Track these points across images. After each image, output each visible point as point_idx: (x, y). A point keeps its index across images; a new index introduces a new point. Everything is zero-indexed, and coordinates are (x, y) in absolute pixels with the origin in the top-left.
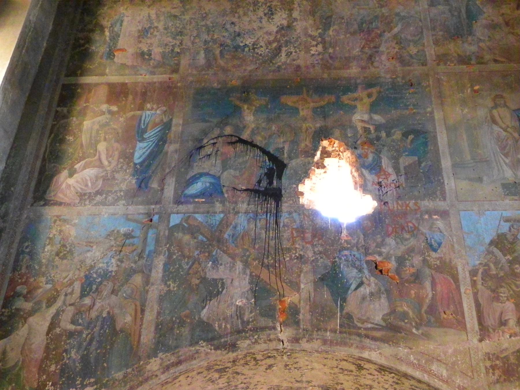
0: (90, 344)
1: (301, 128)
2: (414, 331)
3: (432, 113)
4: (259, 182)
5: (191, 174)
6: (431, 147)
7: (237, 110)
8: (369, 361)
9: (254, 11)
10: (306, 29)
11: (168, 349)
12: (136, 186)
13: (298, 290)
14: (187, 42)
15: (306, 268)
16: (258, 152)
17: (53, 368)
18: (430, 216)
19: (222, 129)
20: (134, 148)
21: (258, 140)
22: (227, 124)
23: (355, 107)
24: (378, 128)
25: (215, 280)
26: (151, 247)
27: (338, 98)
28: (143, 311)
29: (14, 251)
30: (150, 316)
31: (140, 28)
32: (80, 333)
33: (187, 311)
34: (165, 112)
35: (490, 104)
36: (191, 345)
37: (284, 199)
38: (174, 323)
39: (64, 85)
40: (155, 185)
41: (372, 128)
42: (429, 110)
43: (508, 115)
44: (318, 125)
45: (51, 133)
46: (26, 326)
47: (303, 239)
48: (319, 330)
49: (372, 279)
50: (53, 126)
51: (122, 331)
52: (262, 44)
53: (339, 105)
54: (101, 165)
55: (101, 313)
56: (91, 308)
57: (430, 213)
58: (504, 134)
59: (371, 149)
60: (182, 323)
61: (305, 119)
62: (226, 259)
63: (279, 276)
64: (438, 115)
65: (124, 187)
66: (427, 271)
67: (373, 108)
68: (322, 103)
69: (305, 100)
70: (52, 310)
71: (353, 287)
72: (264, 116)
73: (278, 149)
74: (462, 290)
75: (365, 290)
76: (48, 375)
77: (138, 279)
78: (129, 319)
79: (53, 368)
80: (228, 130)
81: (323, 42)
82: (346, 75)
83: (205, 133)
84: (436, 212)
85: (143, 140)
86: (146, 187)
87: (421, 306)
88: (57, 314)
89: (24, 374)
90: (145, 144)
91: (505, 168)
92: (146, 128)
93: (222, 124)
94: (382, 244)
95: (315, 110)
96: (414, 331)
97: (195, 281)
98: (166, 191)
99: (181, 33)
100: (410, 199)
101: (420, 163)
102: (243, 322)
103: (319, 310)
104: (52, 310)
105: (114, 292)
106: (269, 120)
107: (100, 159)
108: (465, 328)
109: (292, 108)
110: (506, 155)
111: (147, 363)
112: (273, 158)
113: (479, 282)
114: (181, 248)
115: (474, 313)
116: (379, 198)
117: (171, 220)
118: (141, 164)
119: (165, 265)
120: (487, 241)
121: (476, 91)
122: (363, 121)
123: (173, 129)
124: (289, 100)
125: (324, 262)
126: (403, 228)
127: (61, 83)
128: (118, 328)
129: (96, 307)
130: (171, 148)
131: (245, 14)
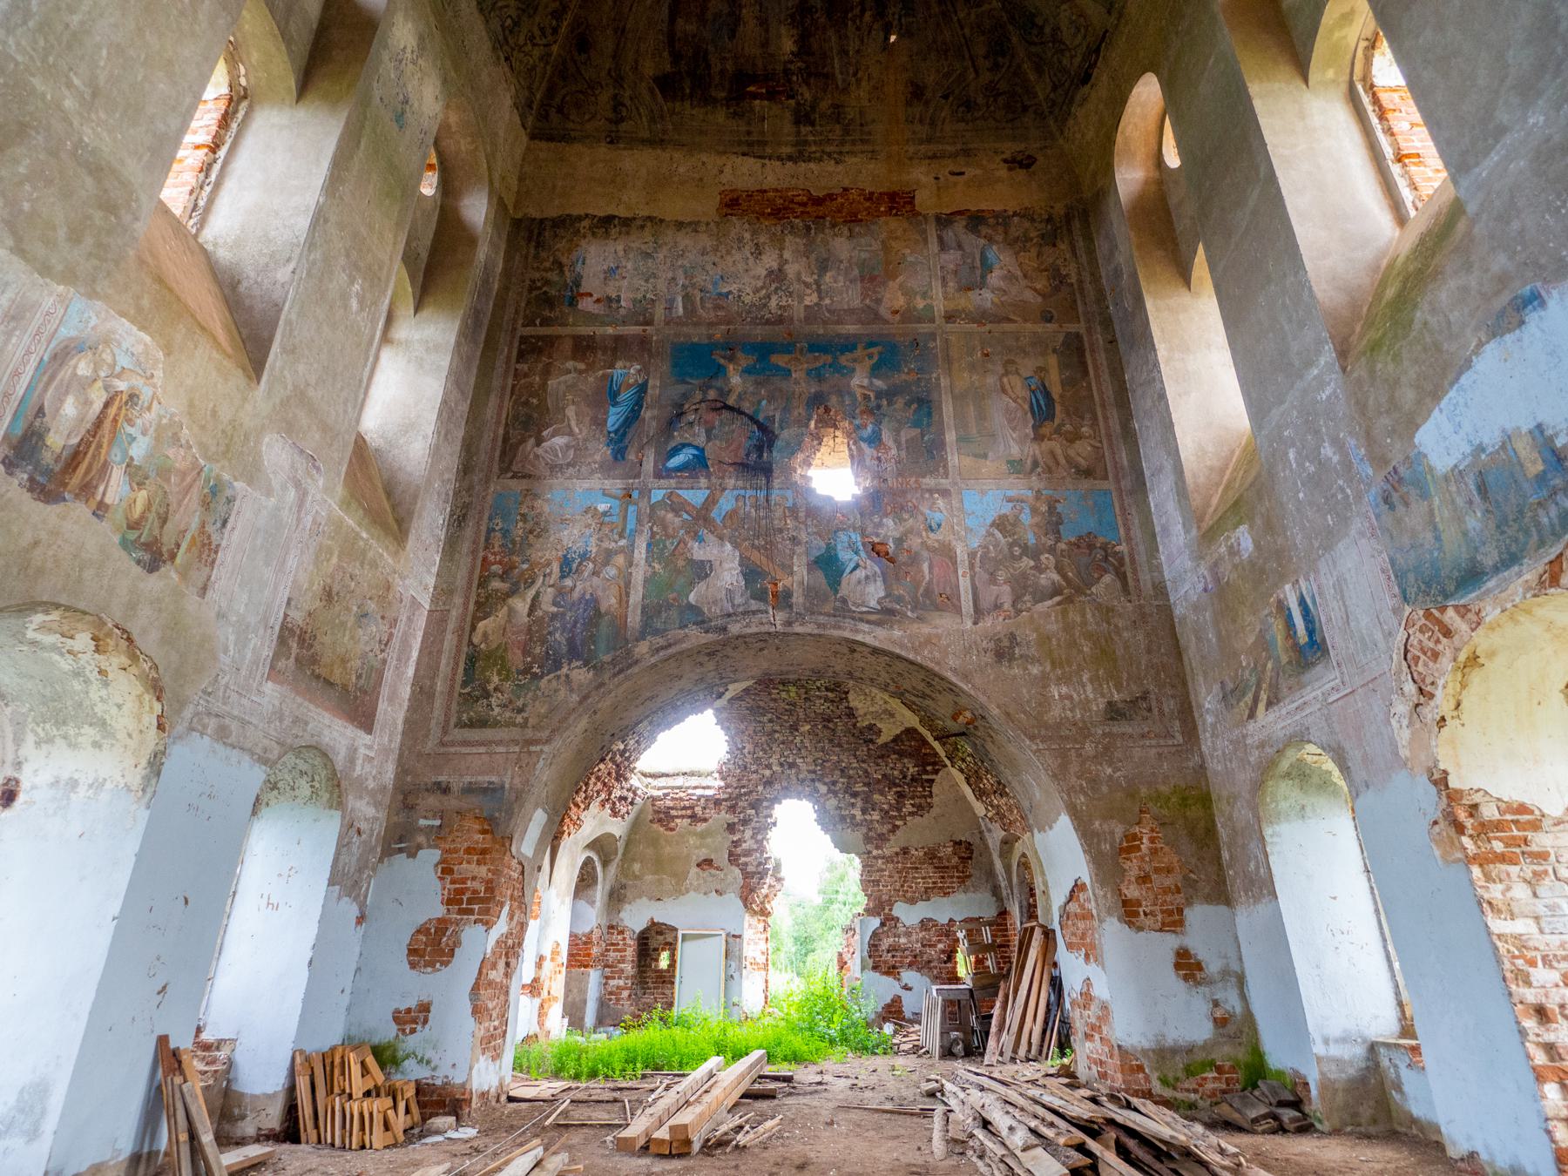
0: (574, 626)
1: (793, 393)
2: (909, 614)
3: (938, 379)
4: (748, 455)
5: (672, 444)
6: (935, 418)
7: (719, 371)
8: (863, 644)
9: (739, 248)
10: (799, 274)
11: (656, 632)
12: (610, 458)
13: (792, 573)
14: (662, 285)
15: (799, 550)
16: (746, 419)
17: (538, 650)
18: (931, 494)
19: (705, 393)
20: (606, 413)
21: (746, 407)
22: (710, 387)
23: (854, 370)
24: (879, 395)
25: (702, 561)
26: (631, 524)
27: (836, 358)
28: (628, 595)
29: (484, 528)
30: (636, 596)
31: (605, 267)
32: (563, 614)
33: (675, 595)
34: (639, 371)
35: (1001, 370)
36: (680, 628)
37: (775, 475)
38: (661, 606)
39: (521, 337)
40: (631, 457)
41: (872, 395)
42: (934, 375)
43: (1019, 384)
44: (813, 390)
45: (512, 394)
46: (506, 608)
47: (796, 518)
48: (813, 613)
49: (868, 562)
50: (514, 386)
51: (606, 614)
52: (749, 290)
53: (837, 368)
54: (571, 433)
55: (584, 594)
56: (573, 589)
57: (931, 491)
58: (1014, 405)
59: (871, 419)
60: (669, 607)
61: (797, 382)
62: (711, 538)
63: (770, 558)
64: (944, 382)
65: (597, 457)
66: (925, 554)
67: (875, 371)
68: (818, 364)
69: (797, 359)
70: (531, 593)
71: (848, 570)
72: (752, 378)
73: (767, 418)
74: (960, 572)
75: (860, 573)
76: (534, 658)
77: (620, 560)
78: (613, 601)
79: (538, 650)
80: (712, 394)
81: (819, 290)
82: (844, 332)
83: (685, 396)
84: (938, 491)
85: (615, 404)
86: (623, 458)
87: (917, 588)
88: (538, 594)
89: (510, 656)
90: (619, 409)
91: (1012, 442)
92: (619, 390)
93: (704, 388)
94: (880, 525)
95: (809, 373)
96: (909, 614)
97: (681, 563)
98: (644, 463)
99: (654, 276)
100: (911, 476)
101: (923, 436)
102: (733, 605)
103: (813, 594)
104: (531, 593)
105: (595, 573)
106: (758, 384)
107: (569, 425)
108: (1400, 1038)
109: (784, 369)
110: (1014, 429)
111: (636, 646)
112: (762, 428)
113: (978, 564)
114: (665, 528)
115: (970, 596)
116: (709, 690)
117: (519, 1029)
118: (616, 432)
119: (649, 545)
120: (989, 522)
121: (987, 355)
122: (862, 387)
123: (650, 391)
124: (779, 360)
125: (819, 545)
126: (902, 508)
127: (519, 334)
128: (603, 610)
129: (577, 589)
130: (647, 414)
131: (728, 253)
